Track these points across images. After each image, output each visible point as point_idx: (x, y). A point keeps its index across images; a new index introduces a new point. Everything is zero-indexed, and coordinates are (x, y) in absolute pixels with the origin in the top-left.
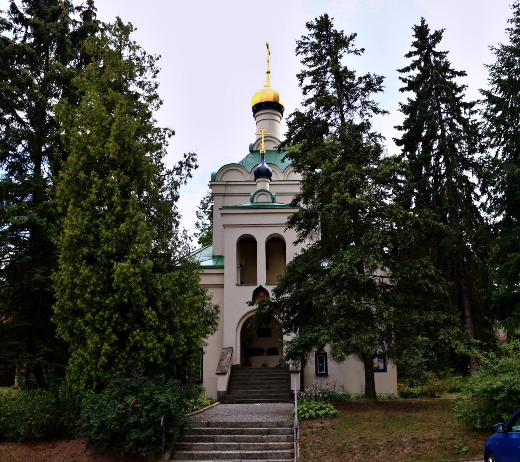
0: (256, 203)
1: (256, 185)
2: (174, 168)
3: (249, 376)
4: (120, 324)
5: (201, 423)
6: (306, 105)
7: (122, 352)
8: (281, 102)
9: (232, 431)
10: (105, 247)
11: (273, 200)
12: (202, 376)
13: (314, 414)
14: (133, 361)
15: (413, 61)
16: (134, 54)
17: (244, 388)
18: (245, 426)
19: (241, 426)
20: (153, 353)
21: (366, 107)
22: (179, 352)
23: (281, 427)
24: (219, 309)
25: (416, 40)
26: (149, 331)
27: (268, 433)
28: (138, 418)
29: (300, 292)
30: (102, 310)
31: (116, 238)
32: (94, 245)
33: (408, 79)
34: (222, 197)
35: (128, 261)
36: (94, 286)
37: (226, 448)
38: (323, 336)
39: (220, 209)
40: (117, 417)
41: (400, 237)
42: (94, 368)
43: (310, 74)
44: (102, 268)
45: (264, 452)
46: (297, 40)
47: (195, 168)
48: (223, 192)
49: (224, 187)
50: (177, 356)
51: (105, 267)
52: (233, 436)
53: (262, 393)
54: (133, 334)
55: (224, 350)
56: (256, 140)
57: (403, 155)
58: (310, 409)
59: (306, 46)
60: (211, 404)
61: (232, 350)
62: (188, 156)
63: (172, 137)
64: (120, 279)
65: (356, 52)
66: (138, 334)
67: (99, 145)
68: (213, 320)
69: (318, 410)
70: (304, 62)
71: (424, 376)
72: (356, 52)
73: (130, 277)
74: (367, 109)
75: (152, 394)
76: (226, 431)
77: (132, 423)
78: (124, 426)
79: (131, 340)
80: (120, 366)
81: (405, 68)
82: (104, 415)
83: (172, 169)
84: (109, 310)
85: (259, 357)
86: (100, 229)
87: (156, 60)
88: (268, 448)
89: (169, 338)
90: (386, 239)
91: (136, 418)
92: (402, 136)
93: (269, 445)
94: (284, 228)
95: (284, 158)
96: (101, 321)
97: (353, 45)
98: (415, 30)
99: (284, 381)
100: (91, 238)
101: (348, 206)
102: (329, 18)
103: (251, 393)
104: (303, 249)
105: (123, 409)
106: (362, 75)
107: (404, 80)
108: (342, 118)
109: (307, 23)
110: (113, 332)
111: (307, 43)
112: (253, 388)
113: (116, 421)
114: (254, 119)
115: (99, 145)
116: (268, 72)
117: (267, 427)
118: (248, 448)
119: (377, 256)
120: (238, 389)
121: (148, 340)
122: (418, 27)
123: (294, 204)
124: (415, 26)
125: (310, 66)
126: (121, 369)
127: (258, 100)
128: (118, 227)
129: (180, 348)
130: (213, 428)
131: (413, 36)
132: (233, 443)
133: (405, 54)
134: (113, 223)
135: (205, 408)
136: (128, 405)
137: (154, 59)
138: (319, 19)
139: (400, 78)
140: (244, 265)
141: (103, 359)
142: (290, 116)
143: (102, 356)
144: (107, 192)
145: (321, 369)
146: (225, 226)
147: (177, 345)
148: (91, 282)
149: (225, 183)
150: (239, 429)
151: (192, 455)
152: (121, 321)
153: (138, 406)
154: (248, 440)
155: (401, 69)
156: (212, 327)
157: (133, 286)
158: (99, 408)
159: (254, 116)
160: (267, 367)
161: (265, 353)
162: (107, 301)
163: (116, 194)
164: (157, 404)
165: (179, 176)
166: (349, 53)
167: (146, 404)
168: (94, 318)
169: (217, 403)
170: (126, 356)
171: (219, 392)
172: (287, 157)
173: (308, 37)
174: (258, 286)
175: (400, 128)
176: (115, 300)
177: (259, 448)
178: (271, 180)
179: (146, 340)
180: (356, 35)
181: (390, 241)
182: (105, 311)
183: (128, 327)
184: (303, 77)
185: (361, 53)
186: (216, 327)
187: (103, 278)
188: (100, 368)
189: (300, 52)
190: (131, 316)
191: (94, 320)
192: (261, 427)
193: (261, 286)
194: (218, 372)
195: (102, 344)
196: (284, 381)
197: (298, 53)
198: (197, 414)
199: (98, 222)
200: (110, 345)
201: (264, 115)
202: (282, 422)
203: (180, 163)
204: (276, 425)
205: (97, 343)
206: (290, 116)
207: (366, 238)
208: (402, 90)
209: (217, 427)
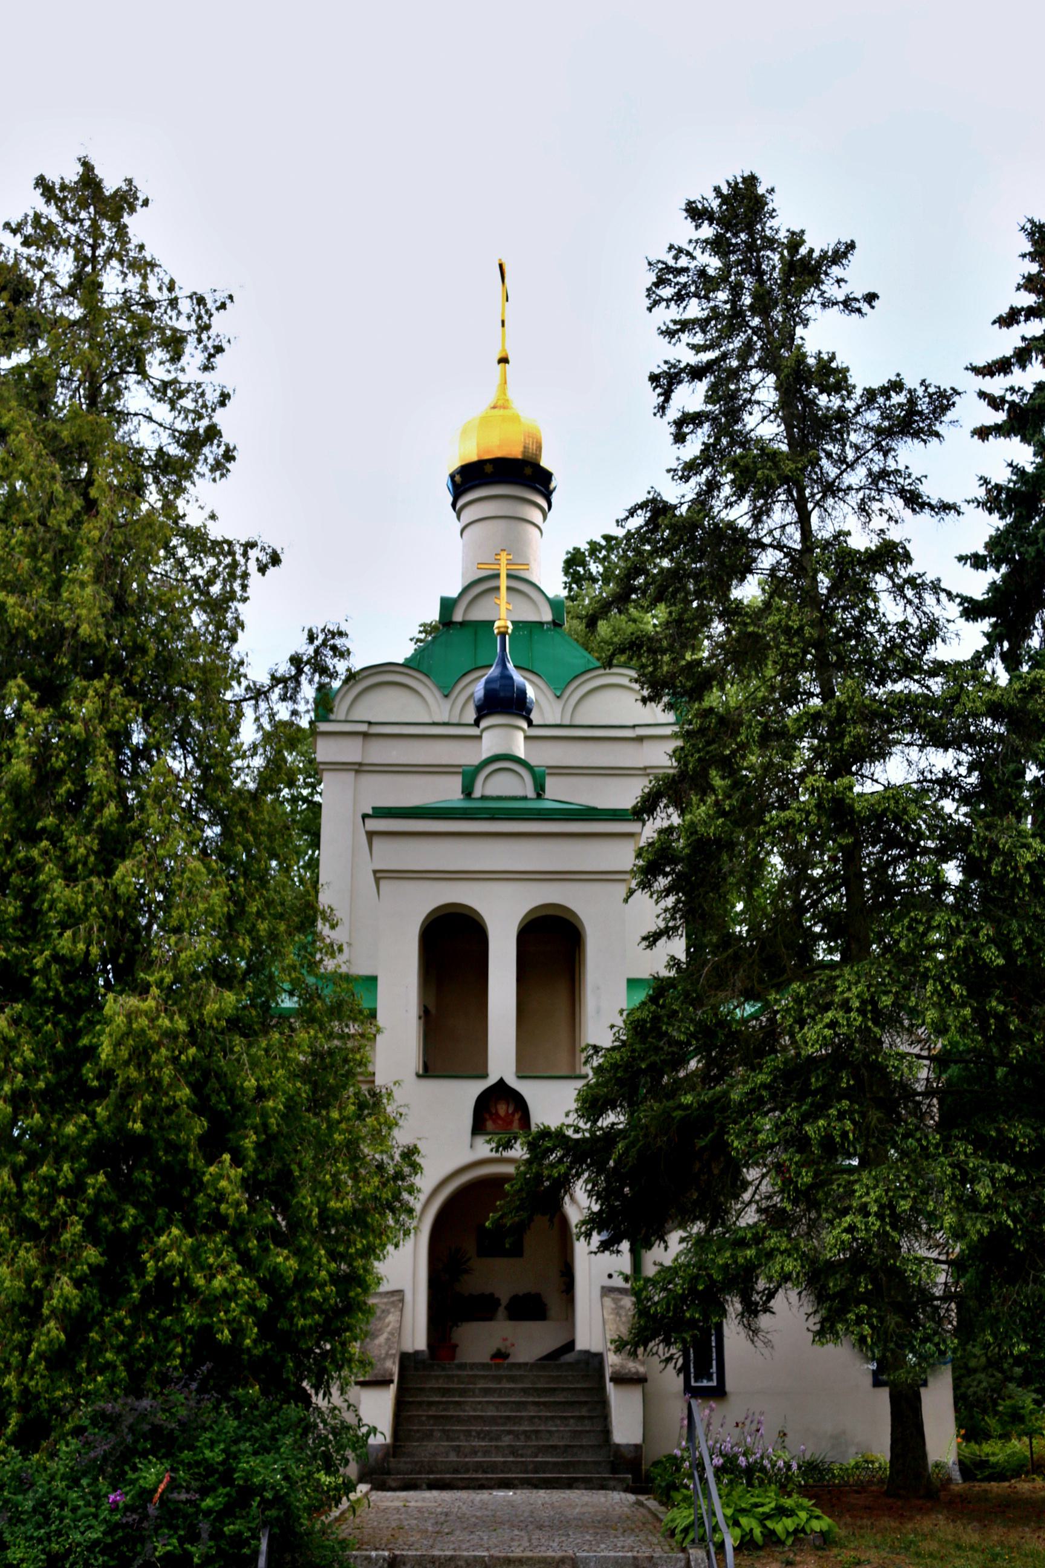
0: (483, 798)
1: (479, 737)
2: (273, 677)
3: (463, 1392)
4: (109, 1208)
5: (368, 1558)
6: (687, 479)
7: (116, 1307)
8: (544, 463)
10: (65, 943)
11: (540, 790)
13: (757, 1532)
14: (151, 1340)
15: (1024, 338)
16: (144, 287)
17: (448, 1436)
20: (226, 1312)
21: (882, 490)
22: (308, 1308)
24: (418, 1159)
25: (1034, 268)
26: (209, 1231)
28: (181, 1541)
29: (681, 1106)
30: (50, 1159)
31: (101, 911)
32: (19, 933)
33: (1009, 397)
34: (352, 774)
35: (155, 991)
36: (26, 1076)
38: (779, 1258)
39: (365, 817)
40: (109, 1540)
41: (1021, 932)
42: (13, 1361)
43: (696, 373)
44: (49, 1012)
46: (653, 260)
48: (357, 759)
49: (358, 742)
50: (302, 1322)
51: (57, 1011)
53: (514, 1451)
56: (459, 590)
57: (989, 652)
58: (742, 1511)
59: (683, 279)
61: (402, 1301)
62: (321, 637)
63: (272, 571)
64: (124, 1054)
65: (847, 304)
66: (175, 1244)
67: (39, 591)
68: (397, 1196)
69: (768, 1516)
70: (669, 334)
71: (1008, 1402)
72: (847, 304)
73: (156, 1047)
74: (886, 496)
75: (231, 1456)
77: (159, 1559)
79: (151, 1264)
80: (109, 1356)
81: (995, 363)
82: (59, 1533)
83: (265, 680)
84: (73, 1159)
85: (487, 1323)
86: (42, 877)
87: (218, 309)
89: (284, 1260)
90: (975, 933)
91: (175, 1541)
92: (985, 587)
94: (621, 890)
96: (42, 1198)
97: (838, 281)
98: (1031, 234)
99: (584, 1412)
100: (11, 909)
101: (853, 821)
102: (761, 190)
103: (474, 1452)
104: (673, 958)
105: (127, 1508)
107: (996, 403)
108: (804, 520)
109: (690, 203)
110: (83, 1236)
111: (686, 270)
112: (480, 1435)
113: (102, 1553)
115: (39, 591)
116: (504, 360)
119: (947, 988)
120: (429, 1436)
121: (210, 1266)
123: (645, 808)
124: (1031, 221)
125: (698, 349)
126: (110, 1366)
127: (472, 455)
128: (109, 872)
129: (316, 1294)
131: (1024, 256)
133: (995, 317)
134: (92, 859)
137: (211, 305)
138: (725, 190)
139: (982, 395)
140: (433, 1011)
141: (53, 1331)
142: (632, 513)
143: (48, 1319)
144: (68, 754)
145: (703, 1372)
147: (304, 1282)
148: (17, 1060)
149: (363, 728)
152: (113, 1197)
155: (981, 363)
157: (166, 1080)
158: (40, 1506)
159: (454, 505)
160: (511, 1360)
161: (501, 1312)
162: (70, 1129)
163: (102, 759)
164: (247, 1492)
165: (290, 705)
166: (824, 305)
167: (204, 1492)
168: (19, 1185)
170: (128, 1322)
173: (690, 248)
175: (978, 562)
176: (96, 1126)
178: (530, 724)
179: (201, 1267)
180: (851, 246)
181: (990, 940)
182: (57, 1162)
183: (135, 1218)
184: (670, 384)
185: (865, 307)
186: (408, 1221)
187: (53, 1046)
188: (36, 1362)
189: (662, 299)
190: (149, 1180)
191: (20, 1194)
193: (501, 1080)
195: (48, 1278)
196: (584, 1412)
197: (656, 303)
199: (35, 853)
200: (78, 1283)
203: (296, 660)
205: (29, 1277)
206: (632, 513)
207: (910, 928)
208: (983, 433)
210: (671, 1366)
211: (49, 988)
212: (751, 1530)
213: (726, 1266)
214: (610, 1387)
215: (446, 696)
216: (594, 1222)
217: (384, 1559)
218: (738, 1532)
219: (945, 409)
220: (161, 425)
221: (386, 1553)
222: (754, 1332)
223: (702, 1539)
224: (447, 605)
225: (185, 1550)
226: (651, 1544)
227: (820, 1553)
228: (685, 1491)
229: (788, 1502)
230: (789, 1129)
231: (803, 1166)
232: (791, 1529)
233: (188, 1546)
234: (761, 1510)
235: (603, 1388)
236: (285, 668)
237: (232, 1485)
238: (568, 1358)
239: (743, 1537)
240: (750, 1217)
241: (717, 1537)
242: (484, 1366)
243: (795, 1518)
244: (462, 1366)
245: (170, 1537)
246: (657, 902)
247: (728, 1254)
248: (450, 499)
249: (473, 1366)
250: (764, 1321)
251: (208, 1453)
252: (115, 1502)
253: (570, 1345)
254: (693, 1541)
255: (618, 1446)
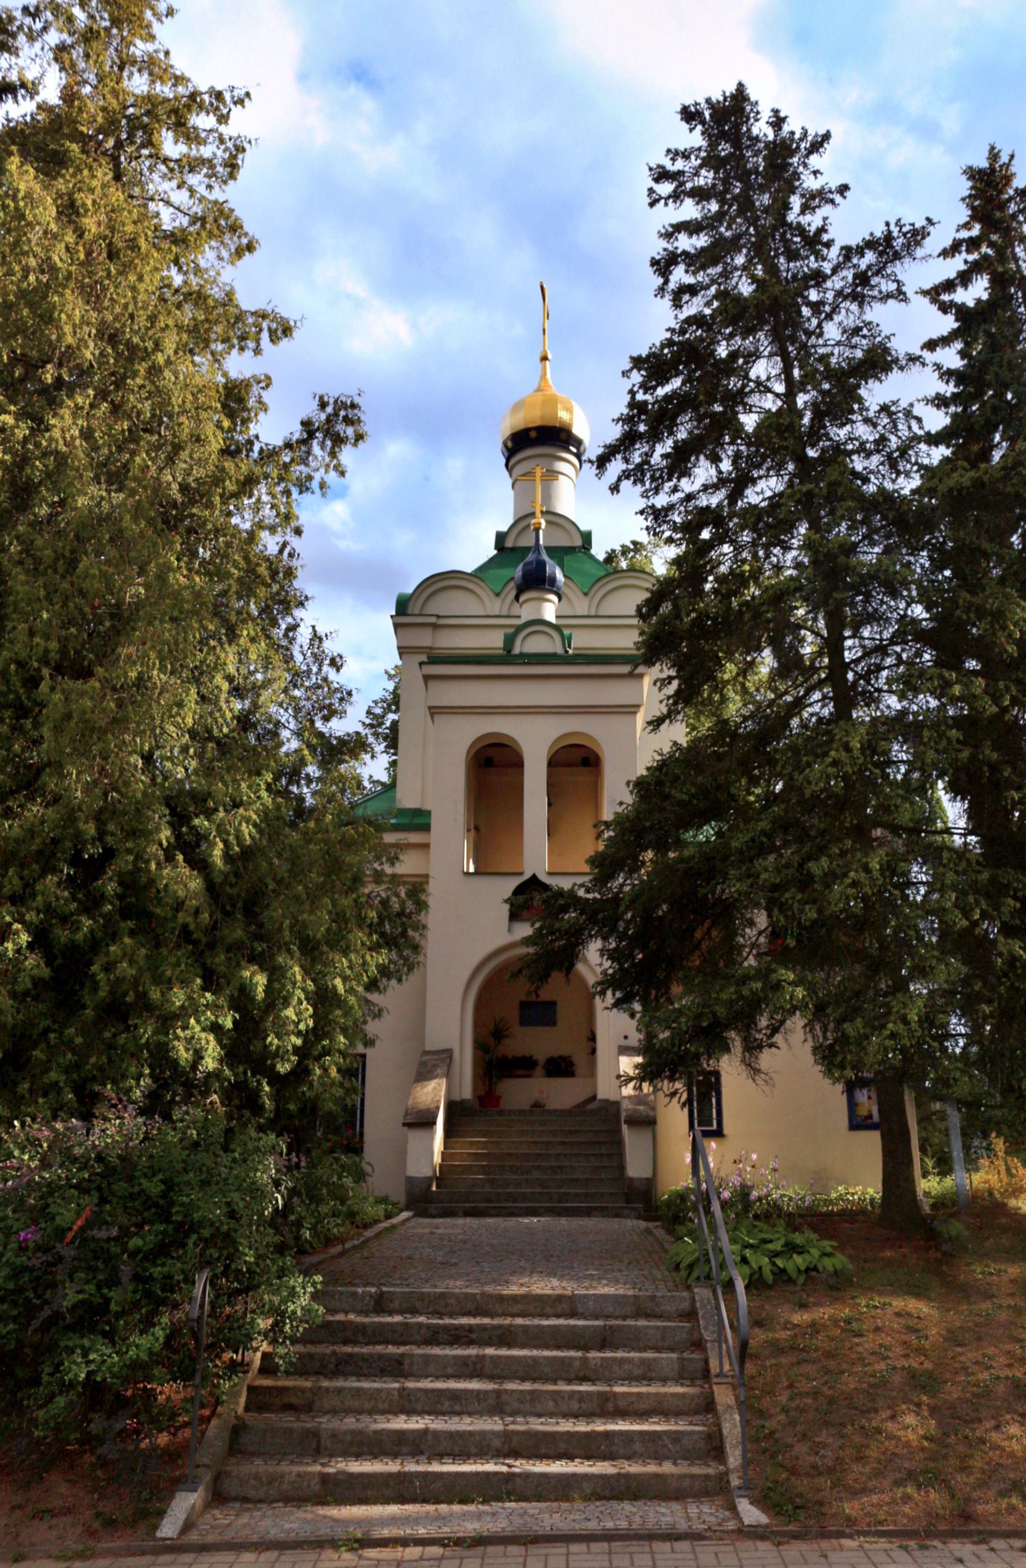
5: (354, 1294)
9: (470, 1329)
12: (362, 1134)
13: (767, 1270)
18: (515, 1309)
19: (499, 1309)
23: (648, 1316)
27: (605, 1340)
37: (446, 1405)
45: (600, 1426)
47: (355, 445)
49: (429, 631)
52: (472, 1351)
54: (107, 954)
55: (426, 1058)
56: (511, 521)
60: (388, 1217)
61: (451, 1057)
68: (404, 934)
76: (446, 1328)
78: (35, 1324)
88: (610, 1406)
91: (91, 1288)
93: (615, 1394)
95: (619, 480)
98: (971, 177)
105: (38, 1248)
106: (854, 241)
114: (506, 473)
116: (544, 358)
117: (596, 1318)
118: (532, 1405)
122: (981, 171)
130: (398, 1319)
132: (474, 1385)
135: (369, 1233)
136: (60, 1233)
146: (434, 711)
149: (433, 620)
150: (496, 1321)
151: (315, 1434)
153: (103, 1234)
154: (530, 1371)
156: (401, 956)
159: (507, 465)
169: (405, 1215)
170: (79, 1040)
171: (410, 1181)
172: (628, 477)
174: (527, 876)
177: (575, 1406)
185: (838, 198)
192: (573, 1314)
193: (534, 877)
194: (409, 1120)
198: (341, 1254)
201: (531, 460)
202: (653, 1298)
203: (306, 424)
204: (628, 1309)
209: (414, 1312)
210: (675, 1099)
211: (10, 691)
212: (760, 1268)
213: (731, 1002)
214: (625, 1128)
215: (498, 595)
216: (608, 983)
217: (371, 1296)
218: (746, 1270)
219: (918, 244)
220: (178, 209)
221: (373, 1290)
222: (754, 1071)
223: (708, 1277)
224: (500, 538)
225: (102, 1296)
226: (655, 1280)
227: (835, 1293)
228: (690, 1224)
229: (798, 1239)
230: (791, 871)
231: (807, 903)
232: (803, 1268)
233: (105, 1291)
234: (770, 1246)
235: (619, 1130)
236: (296, 432)
237: (168, 1221)
238: (591, 1106)
239: (751, 1275)
240: (752, 961)
241: (724, 1275)
242: (522, 1112)
243: (806, 1256)
244: (501, 1113)
245: (87, 1282)
246: (660, 690)
247: (732, 989)
248: (504, 461)
249: (510, 1112)
250: (766, 1059)
251: (145, 1184)
252: (25, 1240)
253: (594, 1098)
254: (698, 1278)
255: (631, 1179)
